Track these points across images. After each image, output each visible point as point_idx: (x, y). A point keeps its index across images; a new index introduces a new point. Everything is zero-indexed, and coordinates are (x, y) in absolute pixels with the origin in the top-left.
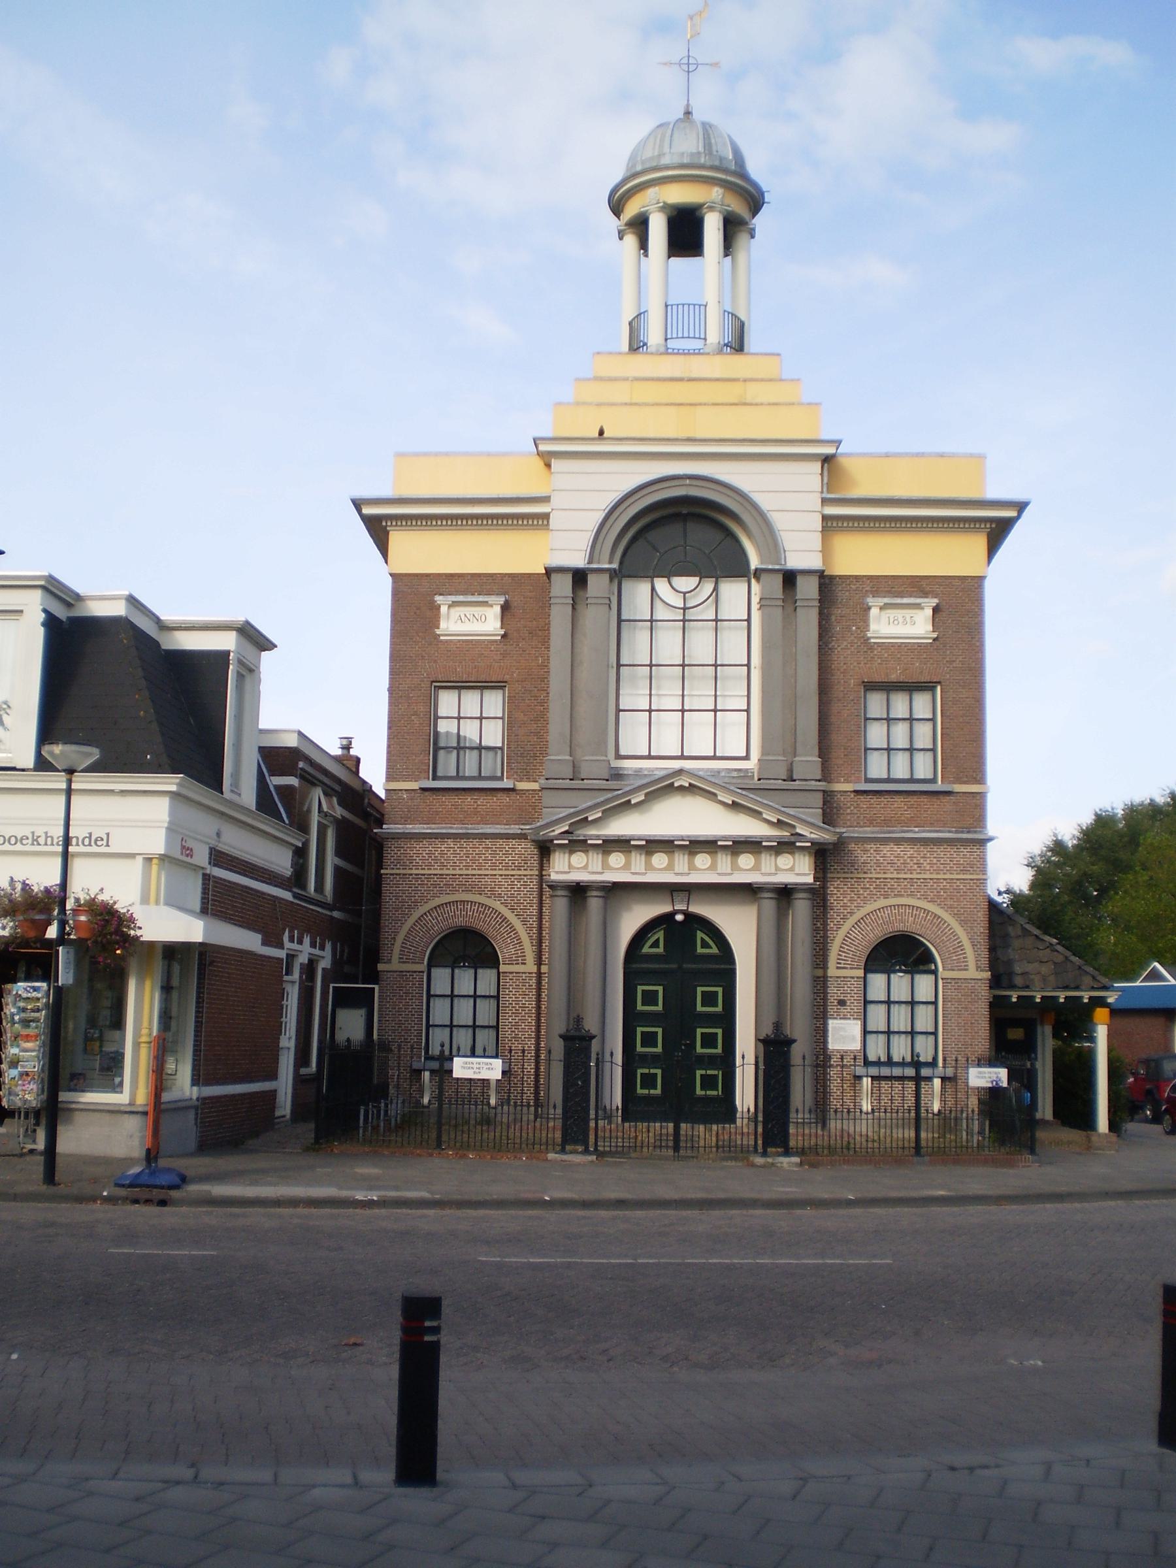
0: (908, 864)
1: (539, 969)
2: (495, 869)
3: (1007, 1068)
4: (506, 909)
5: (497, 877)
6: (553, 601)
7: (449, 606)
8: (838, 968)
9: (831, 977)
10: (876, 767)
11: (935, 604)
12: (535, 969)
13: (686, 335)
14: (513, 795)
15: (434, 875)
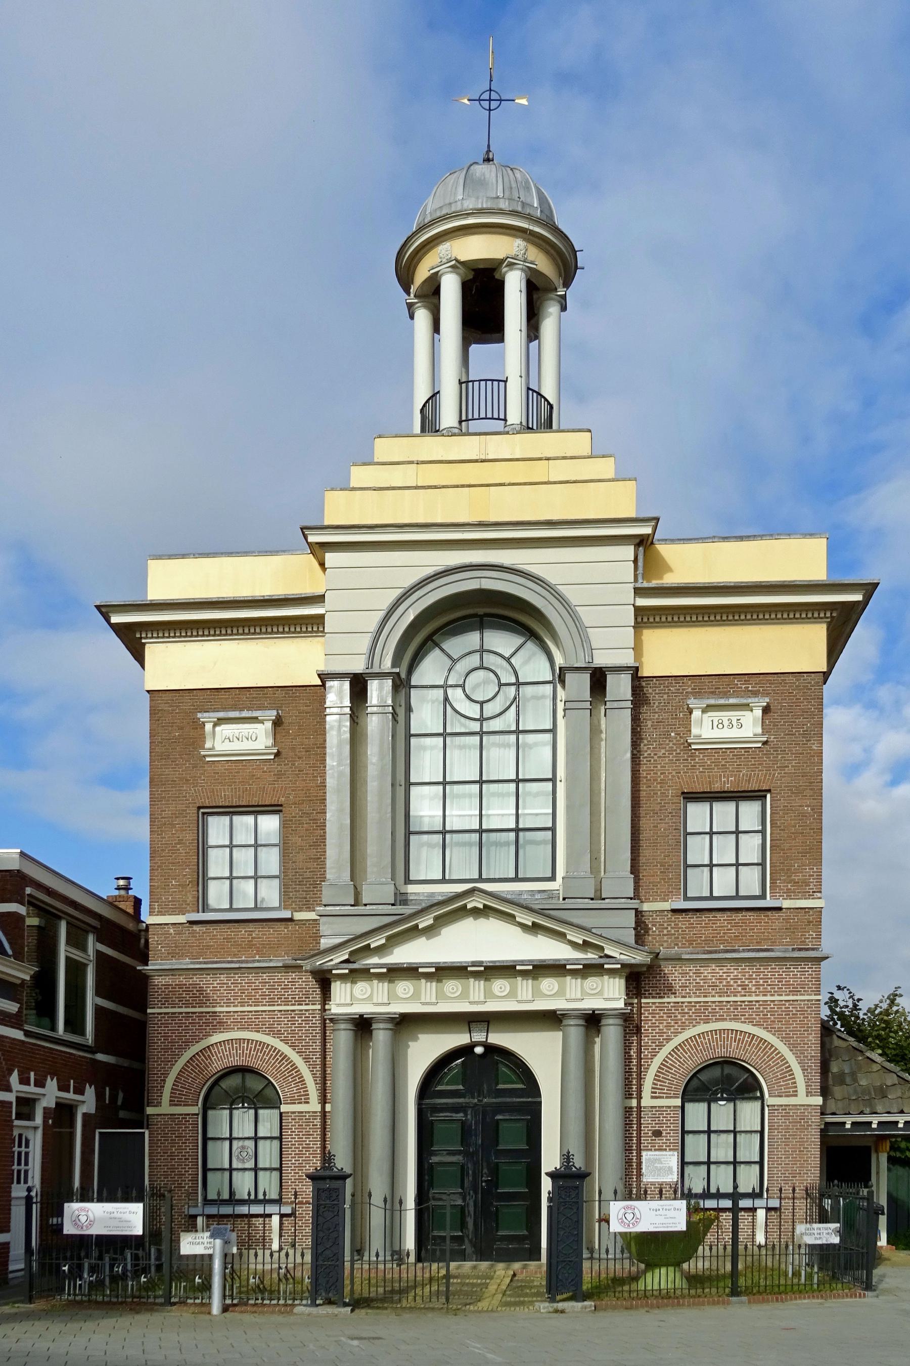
0: (732, 986)
1: (323, 1108)
2: (274, 1005)
4: (286, 1046)
5: (276, 1013)
6: (328, 711)
7: (215, 725)
8: (652, 1097)
9: (645, 1107)
10: (697, 883)
11: (765, 704)
12: (318, 1108)
13: (483, 415)
14: (291, 926)
15: (206, 1012)
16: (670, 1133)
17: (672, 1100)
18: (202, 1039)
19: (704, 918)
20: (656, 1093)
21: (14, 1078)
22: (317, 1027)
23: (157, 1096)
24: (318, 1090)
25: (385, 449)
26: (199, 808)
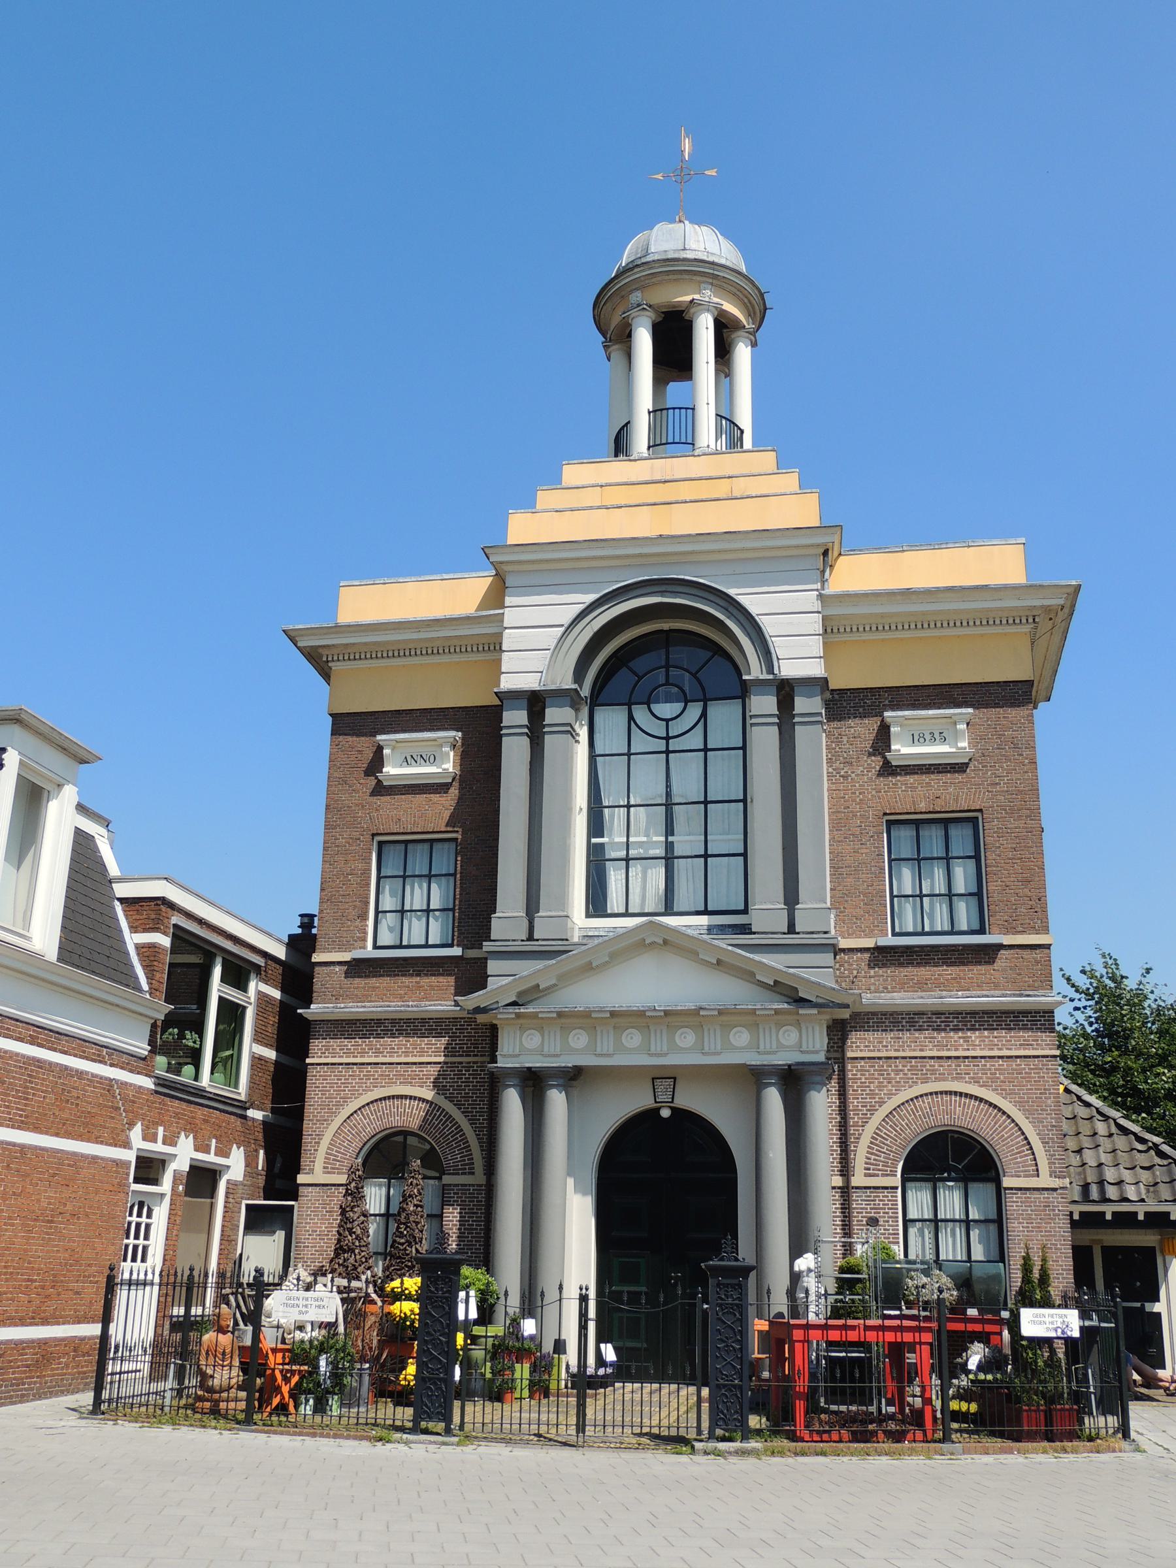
3: (1077, 1307)
8: (866, 1175)
16: (888, 1222)
17: (889, 1178)
18: (362, 1094)
19: (915, 957)
20: (869, 1169)
21: (136, 1134)
22: (486, 1082)
23: (310, 1162)
24: (483, 1158)
25: (573, 473)
26: (373, 835)
